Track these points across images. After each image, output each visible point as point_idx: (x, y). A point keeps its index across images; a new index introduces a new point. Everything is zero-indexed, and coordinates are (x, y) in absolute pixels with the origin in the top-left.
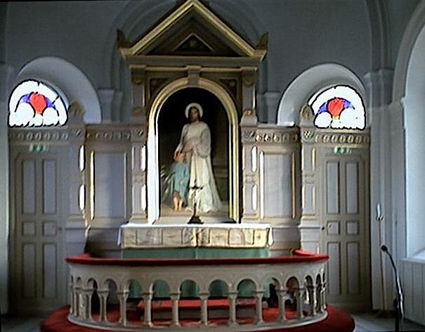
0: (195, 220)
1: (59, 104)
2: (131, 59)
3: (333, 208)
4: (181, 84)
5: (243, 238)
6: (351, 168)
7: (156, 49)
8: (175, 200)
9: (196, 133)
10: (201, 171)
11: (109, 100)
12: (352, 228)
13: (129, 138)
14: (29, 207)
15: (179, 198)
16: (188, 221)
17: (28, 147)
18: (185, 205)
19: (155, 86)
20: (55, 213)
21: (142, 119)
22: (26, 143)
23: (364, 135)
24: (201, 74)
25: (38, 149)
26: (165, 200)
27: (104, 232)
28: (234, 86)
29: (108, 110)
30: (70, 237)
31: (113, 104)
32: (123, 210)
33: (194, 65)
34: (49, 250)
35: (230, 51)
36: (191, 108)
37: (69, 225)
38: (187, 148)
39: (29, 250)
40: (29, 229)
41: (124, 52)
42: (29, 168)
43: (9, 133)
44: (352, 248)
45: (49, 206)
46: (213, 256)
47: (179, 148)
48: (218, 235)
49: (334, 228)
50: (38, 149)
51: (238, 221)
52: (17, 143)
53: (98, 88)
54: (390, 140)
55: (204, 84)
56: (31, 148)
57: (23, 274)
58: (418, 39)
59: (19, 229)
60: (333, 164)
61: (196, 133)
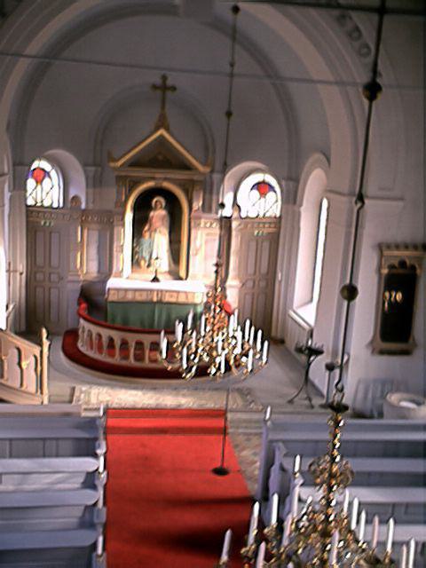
0: (155, 280)
1: (53, 174)
2: (115, 169)
3: (251, 270)
4: (151, 184)
5: (187, 297)
6: (266, 245)
7: (135, 163)
8: (142, 263)
9: (159, 214)
10: (159, 241)
11: (91, 175)
12: (263, 284)
13: (108, 222)
14: (40, 261)
15: (145, 261)
16: (152, 278)
17: (40, 223)
18: (149, 266)
19: (135, 183)
20: (59, 266)
21: (120, 210)
22: (38, 220)
23: (278, 221)
24: (166, 179)
25: (48, 224)
26: (135, 263)
27: (92, 283)
28: (188, 188)
29: (91, 182)
30: (70, 286)
31: (94, 177)
32: (106, 270)
33: (160, 174)
34: (54, 292)
35: (186, 167)
36: (156, 202)
37: (70, 278)
38: (153, 227)
39: (39, 291)
40: (40, 276)
41: (112, 164)
42: (40, 235)
43: (27, 211)
44: (262, 298)
45: (55, 262)
46: (165, 234)
47: (146, 228)
48: (166, 284)
49: (250, 284)
50: (48, 224)
51: (184, 277)
52: (31, 219)
53: (85, 165)
54: (293, 227)
55: (166, 185)
56: (42, 223)
57: (35, 303)
58: (309, 182)
59: (32, 276)
60: (233, 289)
61: (159, 214)
